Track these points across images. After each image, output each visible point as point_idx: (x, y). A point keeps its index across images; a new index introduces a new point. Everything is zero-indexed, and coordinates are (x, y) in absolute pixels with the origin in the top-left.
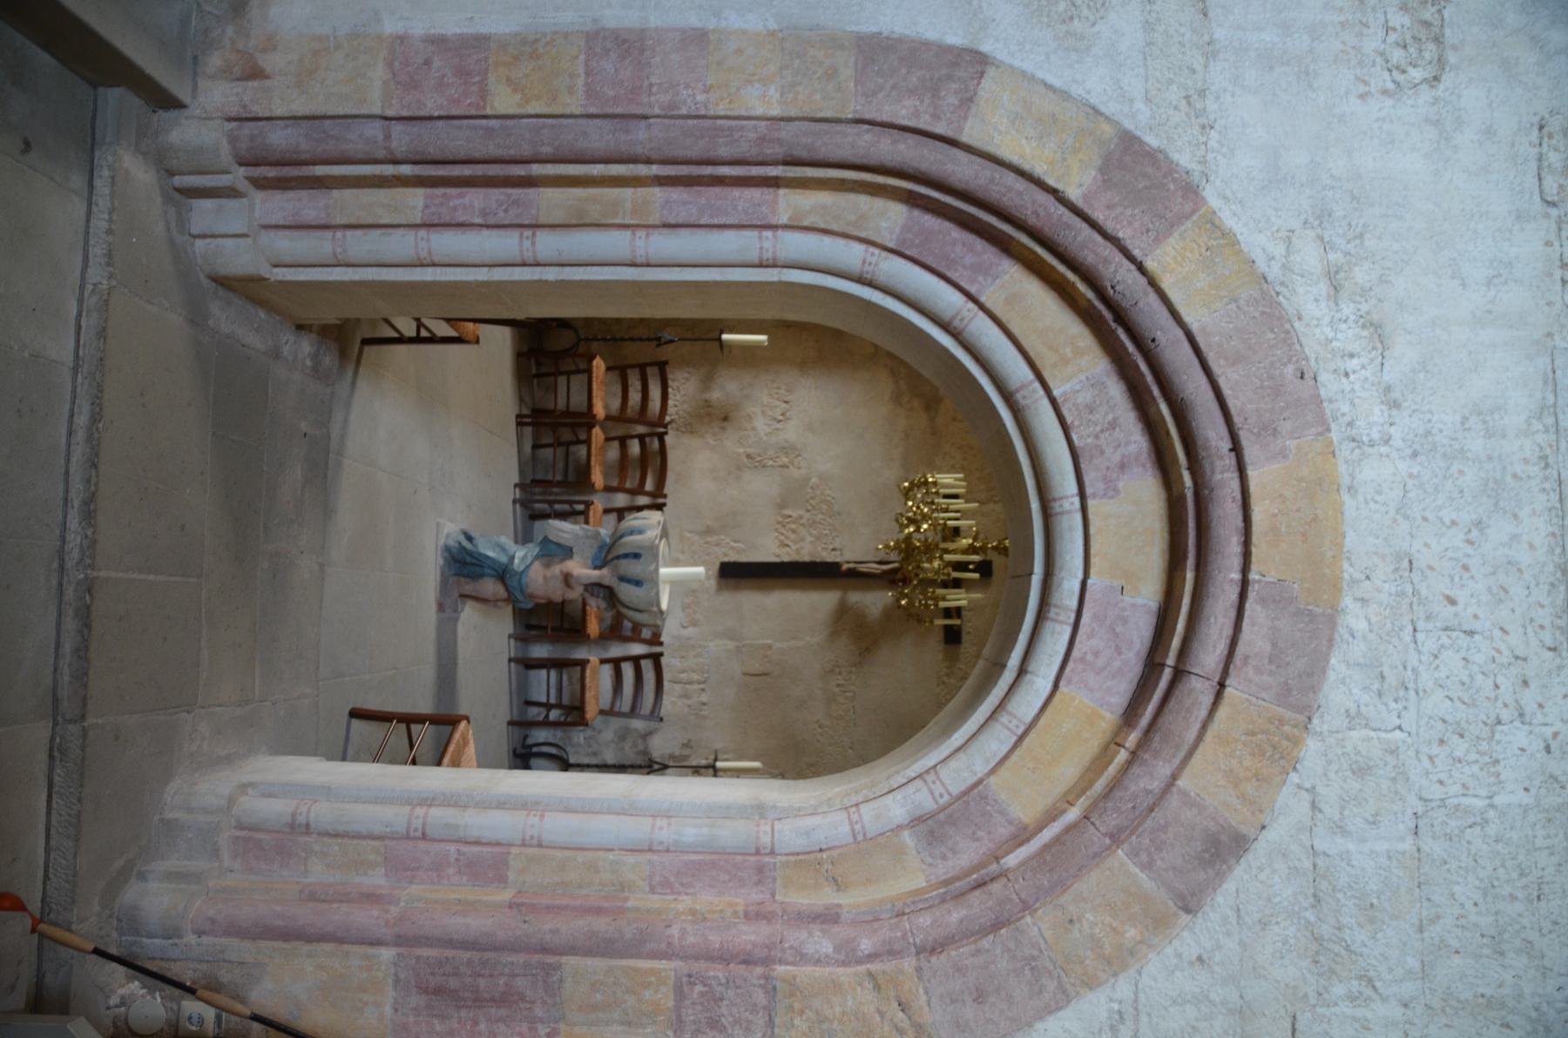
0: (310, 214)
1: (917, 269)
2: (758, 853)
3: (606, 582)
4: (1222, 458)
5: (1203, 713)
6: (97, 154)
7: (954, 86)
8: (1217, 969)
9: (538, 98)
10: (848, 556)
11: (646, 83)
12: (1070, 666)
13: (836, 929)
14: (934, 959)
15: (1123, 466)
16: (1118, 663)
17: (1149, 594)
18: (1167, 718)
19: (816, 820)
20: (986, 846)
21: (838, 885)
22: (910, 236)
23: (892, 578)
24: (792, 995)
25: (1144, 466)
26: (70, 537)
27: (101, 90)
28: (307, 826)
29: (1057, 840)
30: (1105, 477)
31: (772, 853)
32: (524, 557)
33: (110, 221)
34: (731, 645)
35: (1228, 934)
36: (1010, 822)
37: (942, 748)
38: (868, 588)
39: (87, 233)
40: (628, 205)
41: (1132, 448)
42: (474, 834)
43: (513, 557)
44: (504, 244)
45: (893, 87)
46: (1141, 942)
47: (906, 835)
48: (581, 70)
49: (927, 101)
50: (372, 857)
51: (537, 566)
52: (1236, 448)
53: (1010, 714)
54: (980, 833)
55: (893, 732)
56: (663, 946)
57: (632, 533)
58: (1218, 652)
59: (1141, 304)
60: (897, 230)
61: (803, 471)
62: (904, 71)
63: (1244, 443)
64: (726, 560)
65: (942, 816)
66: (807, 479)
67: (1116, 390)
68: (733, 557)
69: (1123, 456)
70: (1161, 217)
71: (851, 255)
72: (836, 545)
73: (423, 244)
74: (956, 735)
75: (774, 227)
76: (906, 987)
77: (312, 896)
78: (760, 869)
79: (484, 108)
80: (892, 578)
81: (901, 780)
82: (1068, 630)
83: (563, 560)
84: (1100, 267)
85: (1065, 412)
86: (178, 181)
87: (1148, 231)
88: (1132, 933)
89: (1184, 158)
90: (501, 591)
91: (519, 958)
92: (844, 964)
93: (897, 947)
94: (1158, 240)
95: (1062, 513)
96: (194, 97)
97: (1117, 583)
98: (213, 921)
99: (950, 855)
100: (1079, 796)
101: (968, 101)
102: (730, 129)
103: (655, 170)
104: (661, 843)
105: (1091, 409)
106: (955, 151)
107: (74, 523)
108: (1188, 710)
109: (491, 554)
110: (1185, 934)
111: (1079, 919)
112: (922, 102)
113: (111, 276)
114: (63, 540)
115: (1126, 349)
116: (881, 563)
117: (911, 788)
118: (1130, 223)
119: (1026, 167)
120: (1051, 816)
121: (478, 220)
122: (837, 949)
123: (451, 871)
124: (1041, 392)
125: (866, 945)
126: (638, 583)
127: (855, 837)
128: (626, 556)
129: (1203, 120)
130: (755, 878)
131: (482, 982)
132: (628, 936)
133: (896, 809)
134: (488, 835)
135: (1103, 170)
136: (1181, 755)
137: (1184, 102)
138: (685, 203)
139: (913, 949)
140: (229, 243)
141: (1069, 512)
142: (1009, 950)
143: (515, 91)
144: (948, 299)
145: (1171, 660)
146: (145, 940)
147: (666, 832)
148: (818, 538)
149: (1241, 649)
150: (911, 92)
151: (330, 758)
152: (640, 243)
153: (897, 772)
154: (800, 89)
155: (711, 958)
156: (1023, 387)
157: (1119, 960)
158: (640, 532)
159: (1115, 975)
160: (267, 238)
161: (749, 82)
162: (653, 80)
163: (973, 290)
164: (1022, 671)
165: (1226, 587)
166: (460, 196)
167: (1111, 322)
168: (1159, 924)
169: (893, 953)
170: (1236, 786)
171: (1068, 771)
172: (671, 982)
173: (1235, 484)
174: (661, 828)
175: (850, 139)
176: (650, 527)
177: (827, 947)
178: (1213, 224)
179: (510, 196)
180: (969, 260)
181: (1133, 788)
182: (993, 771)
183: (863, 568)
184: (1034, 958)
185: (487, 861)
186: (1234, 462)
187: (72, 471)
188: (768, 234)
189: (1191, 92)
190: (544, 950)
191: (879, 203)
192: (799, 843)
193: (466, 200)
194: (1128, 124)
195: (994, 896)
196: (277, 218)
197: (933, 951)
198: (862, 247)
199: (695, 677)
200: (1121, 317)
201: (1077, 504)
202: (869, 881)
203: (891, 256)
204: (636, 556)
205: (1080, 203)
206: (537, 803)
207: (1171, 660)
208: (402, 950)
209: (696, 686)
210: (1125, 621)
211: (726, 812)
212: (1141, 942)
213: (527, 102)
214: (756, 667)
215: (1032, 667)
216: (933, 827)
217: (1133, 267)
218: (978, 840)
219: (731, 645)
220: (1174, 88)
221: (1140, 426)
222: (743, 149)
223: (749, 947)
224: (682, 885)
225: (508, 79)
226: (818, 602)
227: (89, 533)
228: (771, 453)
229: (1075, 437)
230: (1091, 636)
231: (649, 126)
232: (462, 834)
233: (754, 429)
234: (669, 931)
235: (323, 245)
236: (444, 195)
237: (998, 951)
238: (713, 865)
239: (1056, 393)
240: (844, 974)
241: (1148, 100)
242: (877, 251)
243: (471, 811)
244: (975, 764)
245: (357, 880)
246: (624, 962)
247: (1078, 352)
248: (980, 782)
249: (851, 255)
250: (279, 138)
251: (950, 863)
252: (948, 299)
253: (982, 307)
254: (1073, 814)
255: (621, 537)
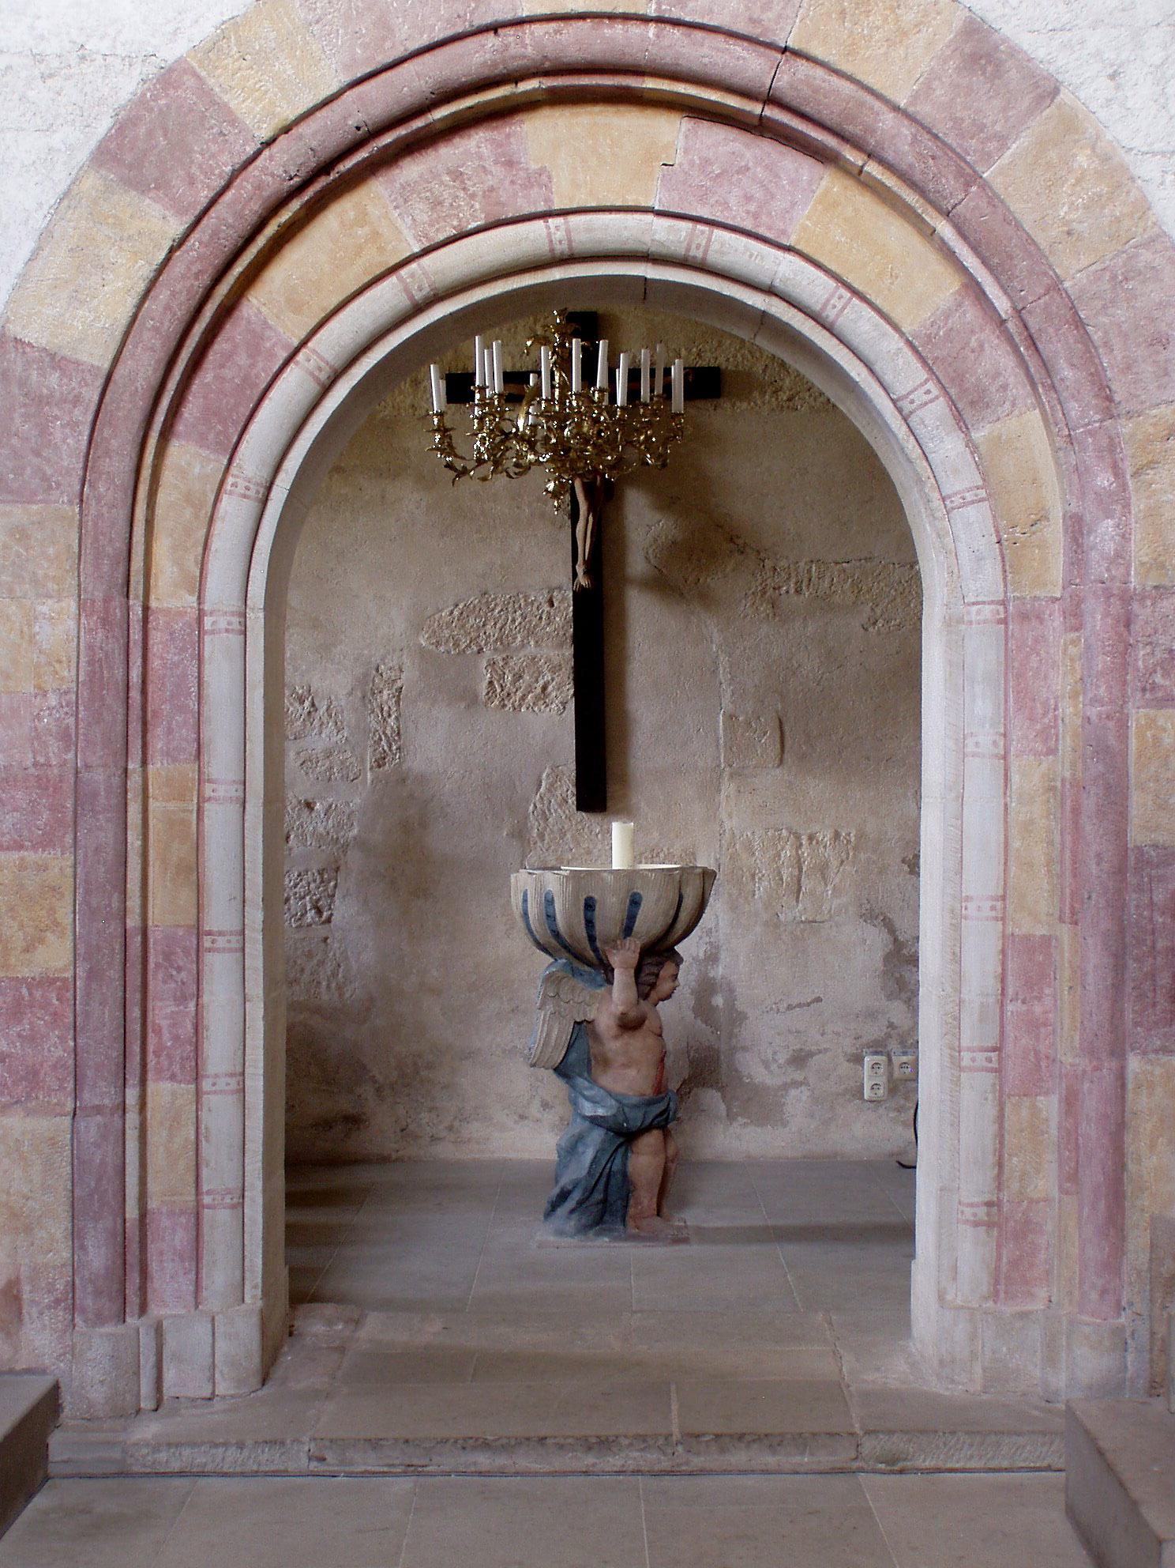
0: (181, 1238)
1: (253, 427)
2: (1005, 621)
3: (633, 957)
4: (507, 47)
5: (819, 72)
6: (135, 1469)
7: (34, 376)
8: (1123, 57)
9: (52, 910)
10: (563, 577)
11: (32, 770)
12: (762, 231)
13: (1088, 518)
14: (1117, 398)
15: (510, 164)
16: (760, 172)
17: (672, 129)
18: (825, 115)
19: (963, 549)
20: (989, 336)
21: (1041, 518)
22: (211, 436)
23: (604, 499)
24: (1162, 566)
25: (508, 136)
26: (631, 1465)
27: (52, 1469)
28: (989, 1204)
29: (975, 249)
30: (524, 187)
31: (1004, 603)
32: (592, 1100)
33: (226, 1445)
34: (728, 788)
35: (1082, 42)
36: (960, 305)
37: (869, 392)
38: (620, 541)
39: (243, 1474)
40: (172, 806)
41: (485, 150)
42: (992, 984)
43: (595, 1121)
44: (219, 969)
45: (37, 454)
46: (1093, 149)
47: (977, 435)
48: (15, 856)
49: (56, 412)
50: (1025, 1113)
51: (607, 1080)
52: (494, 28)
53: (825, 305)
54: (973, 343)
55: (867, 490)
56: (1111, 724)
57: (550, 917)
58: (744, 54)
59: (314, 144)
60: (205, 453)
61: (407, 662)
62: (15, 441)
63: (488, 19)
64: (572, 800)
65: (953, 391)
66: (422, 652)
67: (412, 169)
68: (568, 788)
69: (496, 162)
70: (203, 118)
71: (234, 511)
72: (542, 598)
73: (222, 1083)
74: (853, 374)
75: (201, 615)
76: (1151, 430)
77: (1071, 1178)
78: (1024, 617)
79: (65, 980)
80: (604, 499)
81: (910, 445)
82: (718, 233)
83: (596, 1037)
84: (265, 194)
85: (441, 237)
86: (147, 1404)
87: (221, 133)
88: (1083, 160)
89: (126, 86)
90: (652, 1139)
91: (1132, 898)
92: (1127, 506)
93: (1105, 442)
94: (233, 121)
95: (570, 241)
96: (44, 1372)
97: (659, 171)
98: (1104, 1292)
99: (1001, 381)
100: (923, 221)
101: (55, 361)
102: (91, 663)
103: (134, 765)
104: (995, 743)
105: (437, 203)
106: (116, 377)
107: (614, 1462)
108: (816, 91)
109: (589, 1154)
110: (1082, 95)
111: (1067, 223)
112: (56, 418)
113: (296, 1440)
114: (637, 1472)
115: (364, 160)
116: (574, 517)
117: (920, 431)
118: (213, 156)
119: (142, 286)
120: (949, 255)
121: (192, 1006)
122: (1109, 515)
123: (1038, 1009)
124: (414, 266)
125: (1104, 480)
126: (635, 902)
127: (982, 500)
128: (590, 923)
129: (73, 59)
130: (1034, 623)
131: (1161, 944)
132: (1101, 768)
133: (948, 447)
134: (993, 966)
135: (141, 187)
136: (869, 99)
137: (49, 82)
138: (170, 731)
139: (1108, 423)
140: (222, 1346)
141: (568, 231)
142: (1105, 307)
143: (42, 941)
144: (293, 386)
145: (756, 108)
146: (1128, 1375)
147: (985, 739)
148: (530, 633)
149: (741, 27)
150: (44, 431)
151: (912, 1256)
152: (222, 791)
153: (902, 449)
154: (41, 572)
155: (1125, 666)
156: (407, 290)
157: (1114, 174)
158: (549, 902)
159: (1132, 179)
160: (212, 1301)
161: (33, 636)
162: (29, 763)
163: (283, 355)
164: (770, 291)
165: (666, 42)
166: (158, 1032)
167: (327, 181)
168: (1071, 126)
169: (1112, 447)
170: (905, 34)
171: (895, 233)
172: (1152, 712)
173: (539, 29)
174: (977, 744)
175: (105, 510)
176: (540, 883)
177: (1107, 526)
178: (212, 48)
179: (158, 965)
180: (242, 359)
181: (910, 159)
182: (896, 328)
183: (584, 548)
184: (1114, 277)
185: (1026, 963)
186: (510, 31)
187: (547, 1468)
188: (208, 622)
189: (37, 72)
190: (1120, 871)
191: (167, 476)
192: (991, 570)
193: (164, 1023)
194: (83, 155)
195: (1037, 327)
196: (186, 1285)
197: (1109, 399)
198: (225, 498)
199: (788, 852)
200: (325, 168)
201: (559, 220)
202: (1034, 481)
203: (236, 461)
204: (590, 905)
205: (189, 219)
206: (952, 911)
207: (756, 108)
208: (1128, 1048)
209: (805, 851)
210: (706, 162)
211: (957, 667)
212: (1093, 149)
213: (57, 924)
214: (768, 741)
215: (765, 279)
216: (966, 404)
217: (266, 153)
218: (981, 346)
219: (728, 788)
220: (31, 94)
221: (457, 140)
222: (115, 648)
223: (1109, 621)
224: (1045, 715)
225: (27, 950)
226: (648, 629)
227: (627, 1442)
228: (373, 722)
229: (472, 225)
230: (725, 205)
231: (87, 767)
232: (991, 1000)
233: (328, 754)
234: (1094, 718)
235: (219, 1221)
236: (157, 1054)
237: (1106, 320)
238: (1019, 676)
239: (416, 249)
240: (1139, 504)
241: (50, 129)
242: (230, 480)
243: (965, 996)
244: (888, 348)
245: (1054, 1132)
246: (1132, 770)
247: (362, 218)
248: (910, 344)
249: (234, 511)
250: (98, 1256)
251: (1011, 380)
252: (293, 386)
253: (304, 343)
254: (945, 230)
255: (556, 934)
